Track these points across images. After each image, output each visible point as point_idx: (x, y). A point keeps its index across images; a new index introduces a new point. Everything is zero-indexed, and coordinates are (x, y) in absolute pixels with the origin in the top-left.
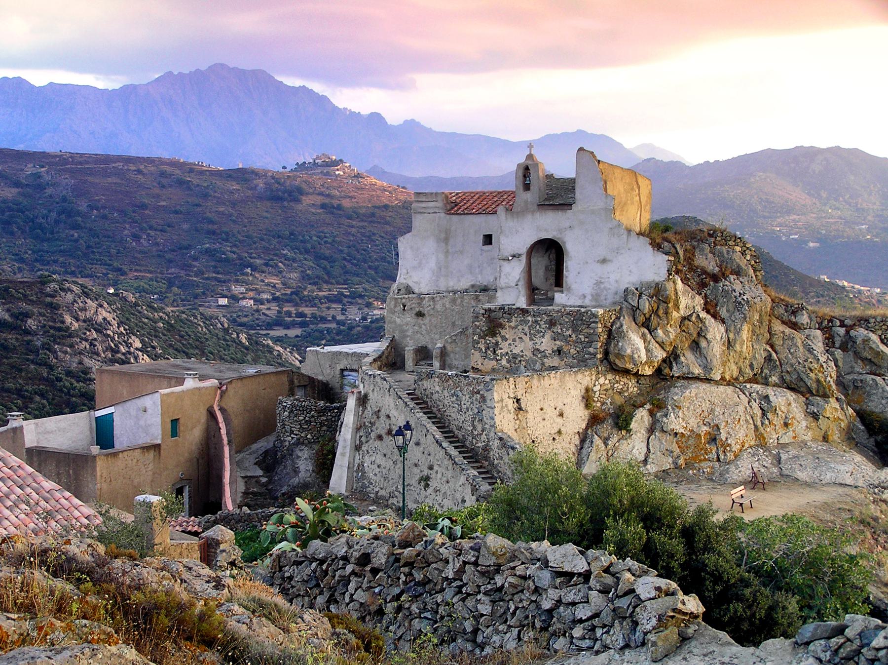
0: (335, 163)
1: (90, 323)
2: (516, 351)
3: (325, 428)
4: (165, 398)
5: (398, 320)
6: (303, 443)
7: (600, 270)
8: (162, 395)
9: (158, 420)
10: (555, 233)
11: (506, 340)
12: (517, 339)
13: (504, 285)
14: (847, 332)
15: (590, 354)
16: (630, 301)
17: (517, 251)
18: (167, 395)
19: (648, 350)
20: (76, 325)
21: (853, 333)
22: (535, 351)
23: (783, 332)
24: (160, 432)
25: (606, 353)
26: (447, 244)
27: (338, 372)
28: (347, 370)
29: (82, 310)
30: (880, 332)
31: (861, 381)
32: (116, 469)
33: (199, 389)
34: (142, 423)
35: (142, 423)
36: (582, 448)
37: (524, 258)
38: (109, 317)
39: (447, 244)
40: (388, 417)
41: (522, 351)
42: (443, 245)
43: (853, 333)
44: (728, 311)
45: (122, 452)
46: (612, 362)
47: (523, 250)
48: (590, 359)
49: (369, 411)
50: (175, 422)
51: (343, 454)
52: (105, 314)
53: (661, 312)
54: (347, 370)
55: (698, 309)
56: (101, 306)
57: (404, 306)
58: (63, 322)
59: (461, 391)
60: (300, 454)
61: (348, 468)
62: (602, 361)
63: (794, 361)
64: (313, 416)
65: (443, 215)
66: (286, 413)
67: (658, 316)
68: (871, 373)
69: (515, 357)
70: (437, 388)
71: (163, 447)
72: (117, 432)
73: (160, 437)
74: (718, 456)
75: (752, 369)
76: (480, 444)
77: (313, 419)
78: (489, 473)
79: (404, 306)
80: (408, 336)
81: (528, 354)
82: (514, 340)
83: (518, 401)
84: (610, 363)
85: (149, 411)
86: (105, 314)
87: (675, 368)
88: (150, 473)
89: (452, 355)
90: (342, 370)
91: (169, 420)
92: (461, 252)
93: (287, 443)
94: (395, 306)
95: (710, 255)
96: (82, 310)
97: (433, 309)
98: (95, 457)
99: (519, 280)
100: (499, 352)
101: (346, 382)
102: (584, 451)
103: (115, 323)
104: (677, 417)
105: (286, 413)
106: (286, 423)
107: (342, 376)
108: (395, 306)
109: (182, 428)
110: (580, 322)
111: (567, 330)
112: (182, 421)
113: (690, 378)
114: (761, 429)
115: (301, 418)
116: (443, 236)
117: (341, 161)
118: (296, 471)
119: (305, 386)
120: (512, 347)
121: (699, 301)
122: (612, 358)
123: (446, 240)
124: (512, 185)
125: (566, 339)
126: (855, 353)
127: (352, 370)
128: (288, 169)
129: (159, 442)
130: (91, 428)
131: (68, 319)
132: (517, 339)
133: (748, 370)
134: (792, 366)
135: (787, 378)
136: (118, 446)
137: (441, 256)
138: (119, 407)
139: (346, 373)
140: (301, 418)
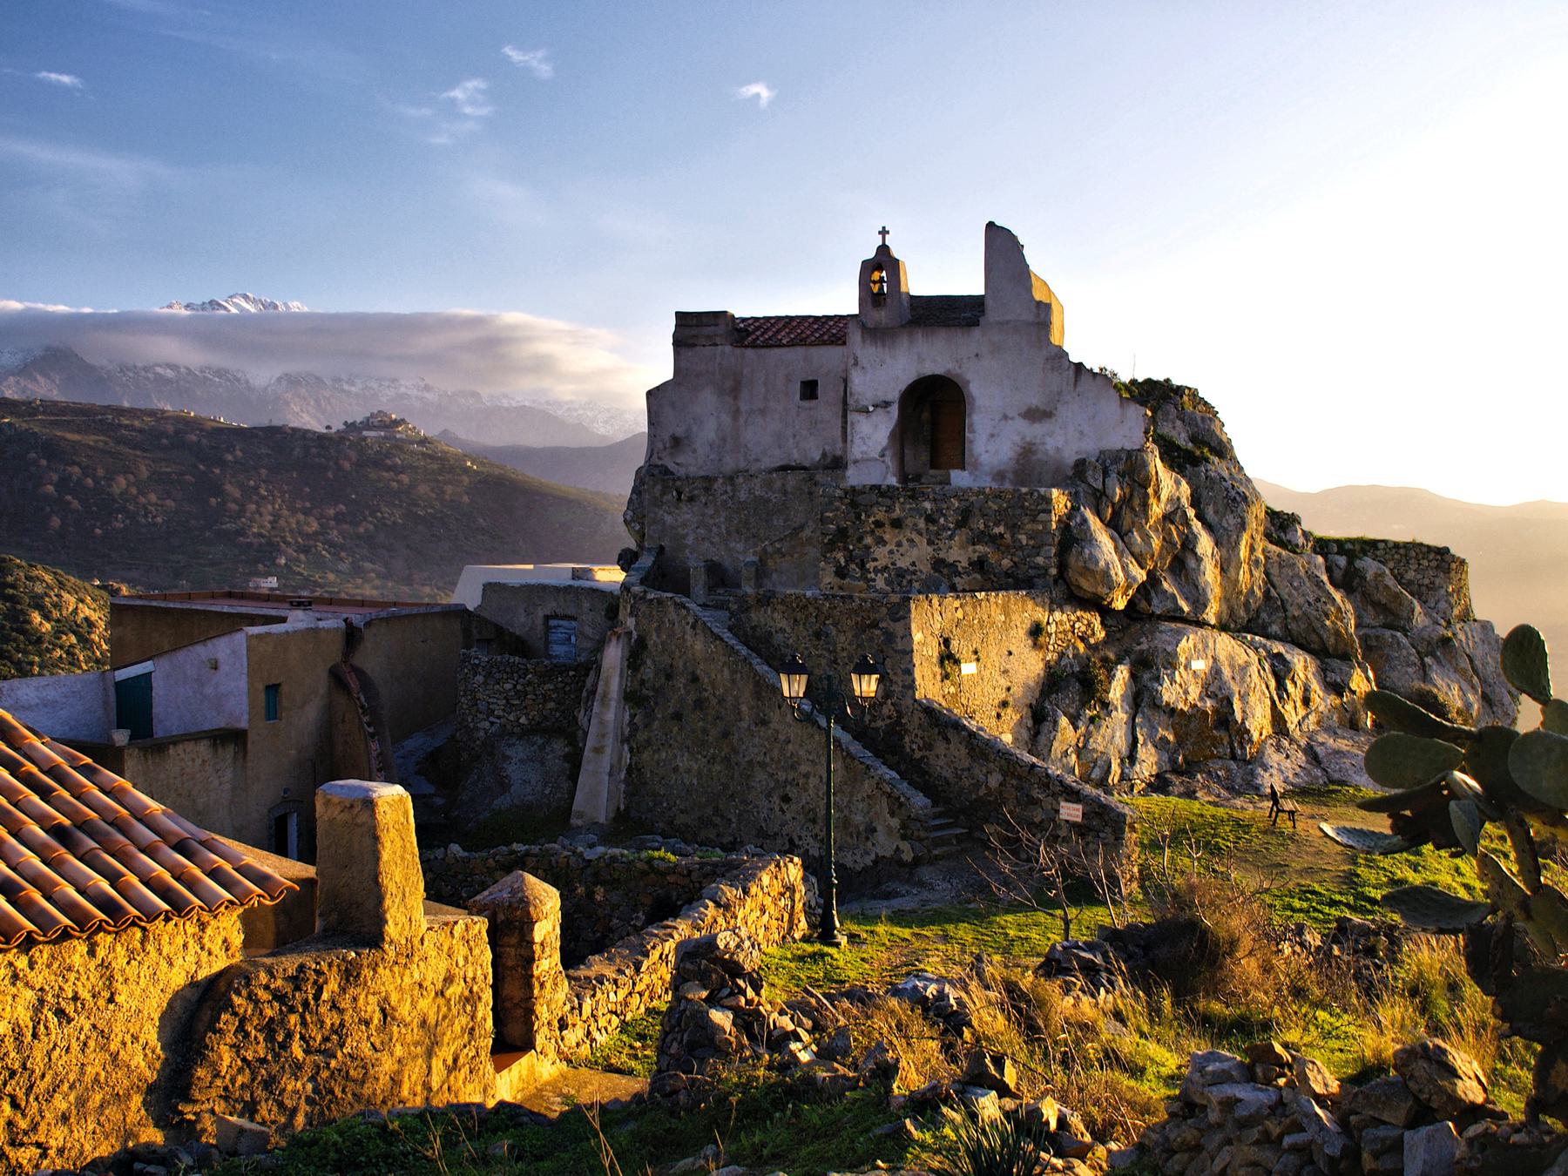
0: (397, 423)
1: (67, 625)
2: (903, 563)
3: (551, 705)
4: (255, 642)
5: (668, 519)
6: (512, 734)
7: (1034, 431)
8: (250, 638)
9: (243, 684)
10: (950, 366)
11: (885, 543)
12: (905, 542)
13: (859, 456)
14: (1350, 563)
15: (1037, 567)
16: (1091, 481)
17: (882, 397)
18: (259, 636)
19: (1125, 568)
20: (48, 626)
21: (1358, 564)
22: (938, 564)
23: (1279, 555)
24: (245, 707)
25: (1063, 567)
26: (735, 398)
27: (540, 621)
28: (556, 616)
29: (55, 606)
30: (1391, 564)
31: (1377, 637)
32: (162, 776)
33: (315, 631)
34: (208, 690)
35: (208, 690)
36: (1037, 733)
37: (894, 410)
38: (94, 616)
39: (735, 398)
40: (695, 679)
41: (913, 564)
42: (728, 399)
43: (1358, 564)
44: (1216, 512)
45: (175, 743)
46: (1069, 584)
47: (894, 394)
48: (1039, 576)
49: (648, 672)
50: (273, 689)
51: (598, 750)
52: (88, 612)
53: (1136, 502)
54: (556, 616)
55: (1185, 502)
56: (82, 601)
57: (680, 494)
58: (30, 622)
59: (835, 624)
60: (508, 753)
61: (610, 775)
62: (1056, 582)
63: (1301, 600)
64: (529, 683)
65: (728, 348)
66: (480, 679)
67: (1133, 509)
68: (1387, 626)
69: (901, 573)
70: (783, 624)
71: (252, 737)
72: (158, 709)
73: (246, 717)
74: (1233, 749)
75: (1247, 610)
76: (879, 723)
77: (529, 689)
78: (916, 773)
79: (680, 494)
80: (686, 546)
81: (925, 568)
82: (899, 544)
83: (947, 642)
84: (1068, 585)
85: (224, 668)
86: (88, 612)
87: (1155, 601)
88: (227, 787)
89: (775, 576)
90: (547, 618)
91: (261, 687)
92: (763, 412)
93: (482, 733)
94: (663, 493)
95: (1178, 423)
96: (55, 606)
97: (732, 498)
98: (121, 750)
99: (884, 449)
100: (870, 565)
101: (553, 637)
102: (1042, 739)
103: (102, 624)
104: (1173, 681)
105: (480, 679)
106: (479, 695)
107: (548, 628)
108: (663, 493)
109: (285, 703)
110: (1018, 512)
111: (997, 524)
112: (285, 689)
113: (1176, 616)
114: (1279, 706)
115: (508, 686)
116: (729, 384)
117: (403, 420)
118: (504, 785)
119: (489, 641)
120: (897, 556)
121: (1185, 490)
122: (1072, 575)
123: (735, 392)
124: (843, 300)
125: (995, 540)
126: (1363, 594)
127: (564, 617)
128: (334, 430)
129: (244, 725)
130: (106, 703)
131: (37, 618)
132: (905, 542)
133: (1242, 613)
134: (1300, 607)
135: (1293, 626)
136: (159, 732)
137: (726, 419)
138: (164, 663)
139: (553, 623)
140: (508, 686)
